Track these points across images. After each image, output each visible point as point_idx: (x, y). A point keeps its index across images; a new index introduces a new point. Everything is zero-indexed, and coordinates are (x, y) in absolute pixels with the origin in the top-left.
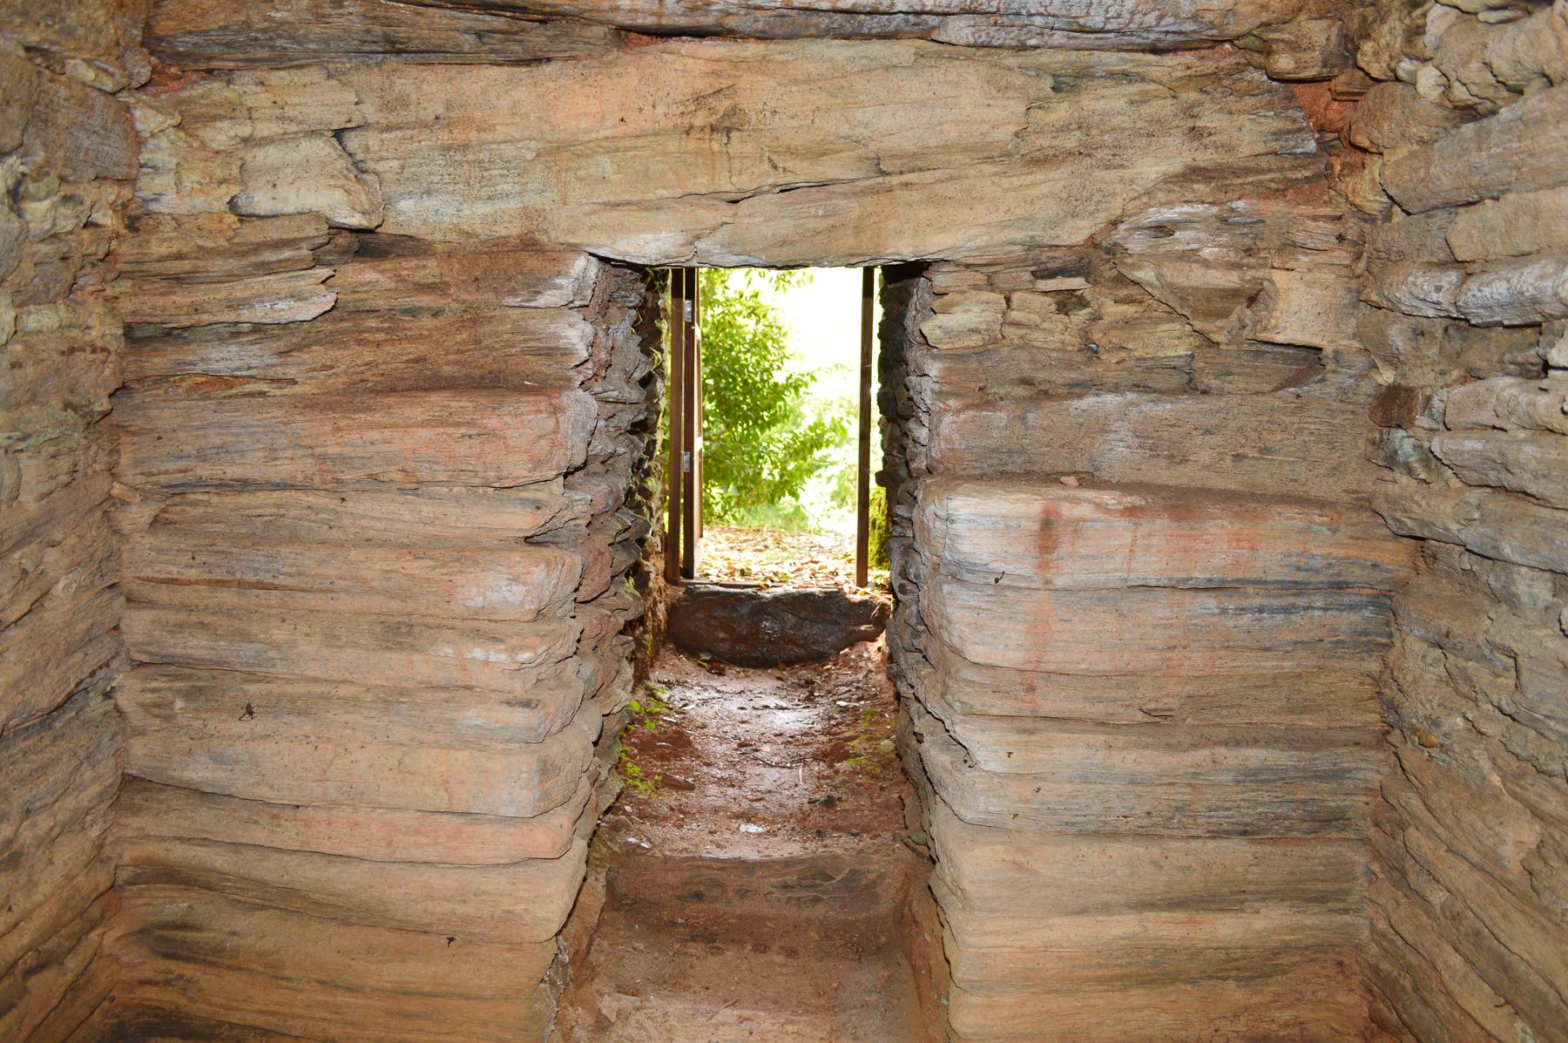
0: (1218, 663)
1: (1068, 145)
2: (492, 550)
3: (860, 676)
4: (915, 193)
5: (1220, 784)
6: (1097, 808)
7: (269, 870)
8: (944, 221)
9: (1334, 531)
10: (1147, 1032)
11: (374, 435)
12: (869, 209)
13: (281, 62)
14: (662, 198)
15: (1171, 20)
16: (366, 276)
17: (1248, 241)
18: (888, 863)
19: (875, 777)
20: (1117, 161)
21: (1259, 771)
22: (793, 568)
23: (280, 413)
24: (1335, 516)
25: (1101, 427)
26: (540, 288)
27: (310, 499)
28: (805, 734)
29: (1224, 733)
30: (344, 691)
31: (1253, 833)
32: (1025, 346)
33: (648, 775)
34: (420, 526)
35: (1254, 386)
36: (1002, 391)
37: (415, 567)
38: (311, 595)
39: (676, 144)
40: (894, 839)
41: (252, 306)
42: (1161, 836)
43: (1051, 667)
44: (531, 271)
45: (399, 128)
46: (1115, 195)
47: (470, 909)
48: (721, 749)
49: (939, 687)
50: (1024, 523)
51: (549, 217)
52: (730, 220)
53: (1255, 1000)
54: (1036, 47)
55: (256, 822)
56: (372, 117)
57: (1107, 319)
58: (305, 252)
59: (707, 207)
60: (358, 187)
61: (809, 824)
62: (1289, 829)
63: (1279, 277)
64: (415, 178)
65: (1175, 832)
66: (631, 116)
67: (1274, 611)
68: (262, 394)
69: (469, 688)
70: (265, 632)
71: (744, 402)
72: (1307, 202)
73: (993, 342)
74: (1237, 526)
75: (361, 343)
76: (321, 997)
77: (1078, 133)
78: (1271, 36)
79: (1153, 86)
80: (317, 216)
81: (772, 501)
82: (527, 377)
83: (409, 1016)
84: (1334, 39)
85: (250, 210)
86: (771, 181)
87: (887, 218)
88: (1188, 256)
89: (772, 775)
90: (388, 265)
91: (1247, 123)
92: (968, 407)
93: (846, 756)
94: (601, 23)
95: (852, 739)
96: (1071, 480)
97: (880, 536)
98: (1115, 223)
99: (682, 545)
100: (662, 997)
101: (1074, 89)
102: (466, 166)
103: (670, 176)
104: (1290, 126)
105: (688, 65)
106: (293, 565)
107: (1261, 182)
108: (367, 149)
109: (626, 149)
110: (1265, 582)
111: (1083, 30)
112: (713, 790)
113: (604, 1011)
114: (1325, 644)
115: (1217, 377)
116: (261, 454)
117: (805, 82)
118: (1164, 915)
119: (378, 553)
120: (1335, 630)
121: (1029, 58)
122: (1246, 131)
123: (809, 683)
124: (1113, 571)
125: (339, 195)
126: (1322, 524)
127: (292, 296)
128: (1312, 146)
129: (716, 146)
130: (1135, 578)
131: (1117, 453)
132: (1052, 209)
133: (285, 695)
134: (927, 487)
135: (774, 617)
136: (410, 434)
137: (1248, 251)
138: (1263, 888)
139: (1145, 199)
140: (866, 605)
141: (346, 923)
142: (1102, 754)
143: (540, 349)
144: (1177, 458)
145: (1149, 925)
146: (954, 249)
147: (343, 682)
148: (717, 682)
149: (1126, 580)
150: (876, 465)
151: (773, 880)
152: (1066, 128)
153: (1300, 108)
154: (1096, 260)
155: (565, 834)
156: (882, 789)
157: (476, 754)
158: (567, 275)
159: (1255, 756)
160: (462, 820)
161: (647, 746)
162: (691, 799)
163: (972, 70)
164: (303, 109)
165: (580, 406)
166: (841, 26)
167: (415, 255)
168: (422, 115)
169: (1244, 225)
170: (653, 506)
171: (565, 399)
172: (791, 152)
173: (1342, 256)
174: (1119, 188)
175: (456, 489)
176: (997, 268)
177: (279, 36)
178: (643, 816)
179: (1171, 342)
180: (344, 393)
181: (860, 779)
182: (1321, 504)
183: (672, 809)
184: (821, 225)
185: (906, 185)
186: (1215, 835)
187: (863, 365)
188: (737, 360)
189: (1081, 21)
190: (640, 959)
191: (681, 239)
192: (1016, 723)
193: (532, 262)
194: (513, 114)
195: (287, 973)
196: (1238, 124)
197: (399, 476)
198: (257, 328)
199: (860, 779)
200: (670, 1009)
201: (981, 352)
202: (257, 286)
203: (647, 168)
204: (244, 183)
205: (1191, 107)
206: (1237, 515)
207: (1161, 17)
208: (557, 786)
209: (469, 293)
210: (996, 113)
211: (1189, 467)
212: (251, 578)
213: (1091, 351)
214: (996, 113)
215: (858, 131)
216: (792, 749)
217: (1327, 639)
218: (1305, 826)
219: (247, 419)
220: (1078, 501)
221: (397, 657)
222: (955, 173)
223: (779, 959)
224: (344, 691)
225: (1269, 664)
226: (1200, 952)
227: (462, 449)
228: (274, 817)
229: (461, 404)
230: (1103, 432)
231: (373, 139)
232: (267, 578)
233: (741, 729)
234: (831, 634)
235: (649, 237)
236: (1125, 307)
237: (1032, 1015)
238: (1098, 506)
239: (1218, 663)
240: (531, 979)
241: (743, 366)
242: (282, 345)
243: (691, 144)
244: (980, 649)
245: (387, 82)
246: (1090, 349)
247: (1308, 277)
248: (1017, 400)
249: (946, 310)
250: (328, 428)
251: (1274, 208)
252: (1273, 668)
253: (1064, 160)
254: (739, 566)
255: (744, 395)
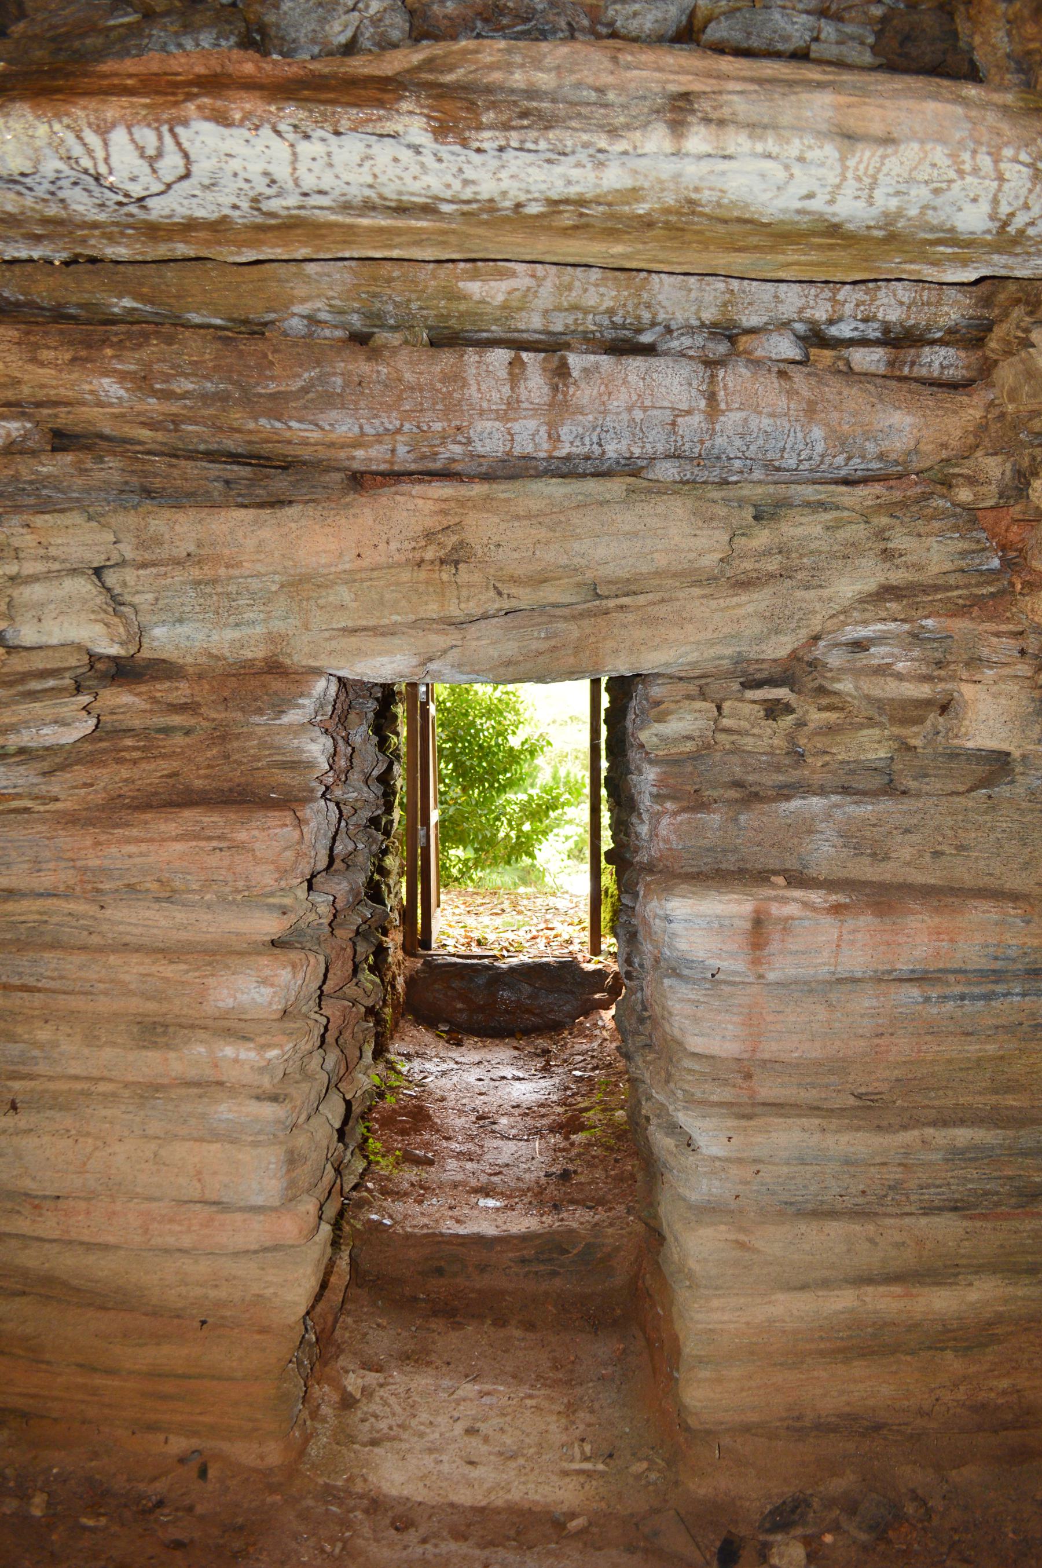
0: (924, 1048)
1: (770, 568)
2: (241, 954)
3: (595, 1045)
4: (630, 615)
5: (930, 1164)
6: (813, 1188)
7: (30, 1259)
8: (657, 640)
9: (1028, 922)
10: (871, 1402)
11: (132, 849)
12: (588, 631)
13: (45, 507)
14: (395, 624)
15: (859, 461)
16: (122, 700)
17: (938, 655)
18: (622, 1236)
19: (610, 1149)
20: (815, 582)
21: (962, 1152)
22: (529, 936)
23: (44, 828)
24: (1028, 909)
25: (807, 827)
26: (284, 708)
27: (72, 906)
28: (542, 1105)
29: (933, 1114)
30: (103, 1087)
31: (963, 1209)
32: (736, 750)
33: (389, 1151)
34: (175, 932)
35: (950, 787)
36: (715, 794)
37: (170, 971)
38: (73, 997)
39: (409, 575)
40: (628, 1213)
41: (19, 732)
42: (876, 1214)
43: (767, 1056)
44: (276, 693)
45: (154, 565)
46: (814, 612)
47: (222, 1294)
48: (460, 1122)
49: (663, 1074)
50: (737, 922)
51: (292, 642)
52: (459, 643)
53: (972, 1370)
54: (736, 483)
55: (18, 1212)
56: (129, 555)
57: (812, 726)
58: (68, 682)
59: (438, 632)
60: (117, 620)
61: (546, 1197)
62: (997, 1204)
63: (968, 691)
64: (167, 608)
65: (890, 1210)
66: (367, 552)
67: (974, 998)
68: (27, 810)
69: (220, 1084)
70: (29, 1033)
71: (480, 765)
72: (991, 619)
73: (705, 749)
74: (937, 920)
75: (119, 761)
76: (80, 1380)
77: (779, 557)
78: (951, 471)
79: (846, 514)
80: (78, 647)
81: (509, 863)
82: (272, 790)
83: (164, 1397)
84: (1008, 473)
85: (17, 642)
86: (496, 606)
87: (604, 639)
88: (882, 671)
89: (509, 1148)
90: (143, 688)
91: (935, 545)
92: (684, 810)
93: (582, 1128)
94: (338, 470)
95: (586, 1110)
96: (780, 880)
97: (613, 904)
98: (816, 638)
99: (419, 911)
100: (404, 1373)
101: (774, 517)
102: (215, 598)
103: (404, 603)
104: (974, 546)
105: (417, 507)
106: (56, 969)
107: (949, 598)
108: (124, 584)
109: (362, 580)
110: (966, 971)
111: (778, 469)
112: (452, 1164)
113: (350, 1388)
114: (1025, 1028)
115: (915, 778)
116: (26, 866)
117: (525, 517)
118: (882, 1289)
119: (135, 958)
120: (1033, 1014)
121: (731, 492)
122: (934, 553)
123: (546, 1052)
124: (821, 966)
125: (99, 628)
126: (1015, 917)
127: (56, 722)
128: (996, 563)
129: (445, 577)
130: (842, 972)
131: (824, 852)
132: (757, 627)
133: (46, 1091)
134: (647, 885)
135: (511, 987)
136: (165, 847)
137: (939, 664)
138: (975, 1261)
139: (842, 617)
140: (600, 974)
141: (103, 1308)
142: (817, 1137)
143: (284, 762)
144: (879, 856)
145: (868, 1299)
146: (666, 665)
147: (102, 1079)
148: (455, 1054)
149: (834, 973)
150: (607, 843)
151: (511, 1255)
152: (767, 553)
153: (984, 530)
154: (796, 672)
155: (313, 1219)
156: (616, 1161)
157: (227, 1146)
158: (309, 695)
159: (962, 1135)
160: (214, 1208)
161: (388, 1121)
162: (430, 1175)
163: (679, 503)
164: (65, 549)
165: (319, 817)
166: (558, 468)
167: (169, 678)
168: (175, 552)
169: (934, 640)
170: (391, 882)
171: (307, 812)
172: (514, 580)
173: (1024, 669)
174: (818, 606)
175: (208, 897)
176: (709, 680)
177: (45, 487)
178: (385, 1192)
179: (872, 746)
180: (102, 808)
181: (595, 1151)
182: (1015, 897)
183: (413, 1185)
184: (544, 646)
185: (622, 607)
186: (929, 1210)
187: (592, 740)
188: (472, 724)
189: (777, 464)
190: (383, 1338)
191: (415, 661)
192: (735, 1109)
193: (277, 684)
194: (258, 552)
195: (48, 1357)
196: (926, 545)
197: (155, 886)
198: (22, 751)
199: (595, 1151)
200: (413, 1386)
201: (695, 757)
202: (23, 712)
203: (382, 597)
204: (12, 618)
205: (883, 531)
206: (937, 910)
207: (849, 459)
208: (304, 1173)
209: (219, 712)
210: (702, 542)
211: (890, 865)
212: (16, 981)
213: (799, 757)
214: (702, 542)
215: (577, 560)
216: (529, 1121)
217: (1026, 1023)
218: (1013, 1201)
219: (13, 835)
220: (785, 901)
221: (153, 1056)
222: (666, 596)
223: (518, 1333)
224: (103, 1087)
225: (973, 1049)
226: (917, 1325)
227: (213, 861)
228: (36, 1207)
229: (212, 819)
230: (810, 832)
231: (130, 575)
232: (31, 982)
233: (479, 1101)
234: (567, 1002)
235: (385, 660)
236: (828, 714)
237: (759, 1388)
238: (805, 904)
239: (924, 1048)
240: (279, 1360)
241: (478, 731)
242: (45, 765)
243: (423, 575)
244: (699, 1040)
245: (143, 523)
246: (796, 752)
247: (994, 689)
248: (731, 802)
249: (661, 719)
250: (89, 842)
251: (960, 625)
252: (976, 1051)
253: (766, 583)
254: (476, 935)
255: (480, 759)
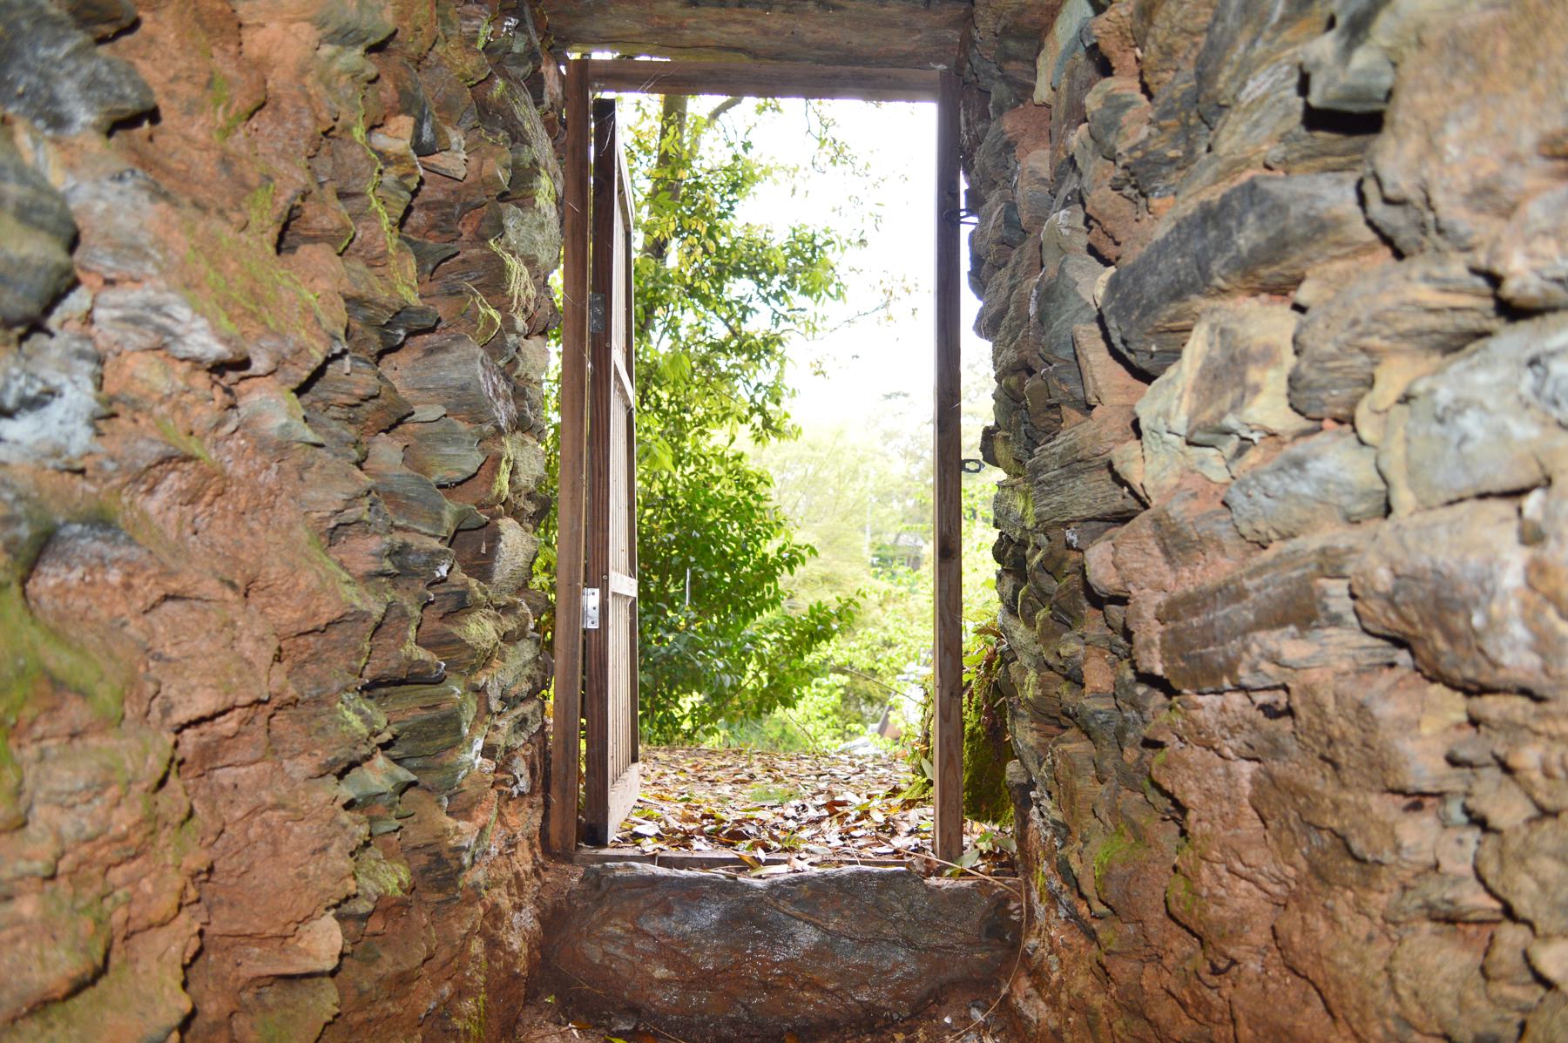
22: (820, 714)
81: (758, 715)
